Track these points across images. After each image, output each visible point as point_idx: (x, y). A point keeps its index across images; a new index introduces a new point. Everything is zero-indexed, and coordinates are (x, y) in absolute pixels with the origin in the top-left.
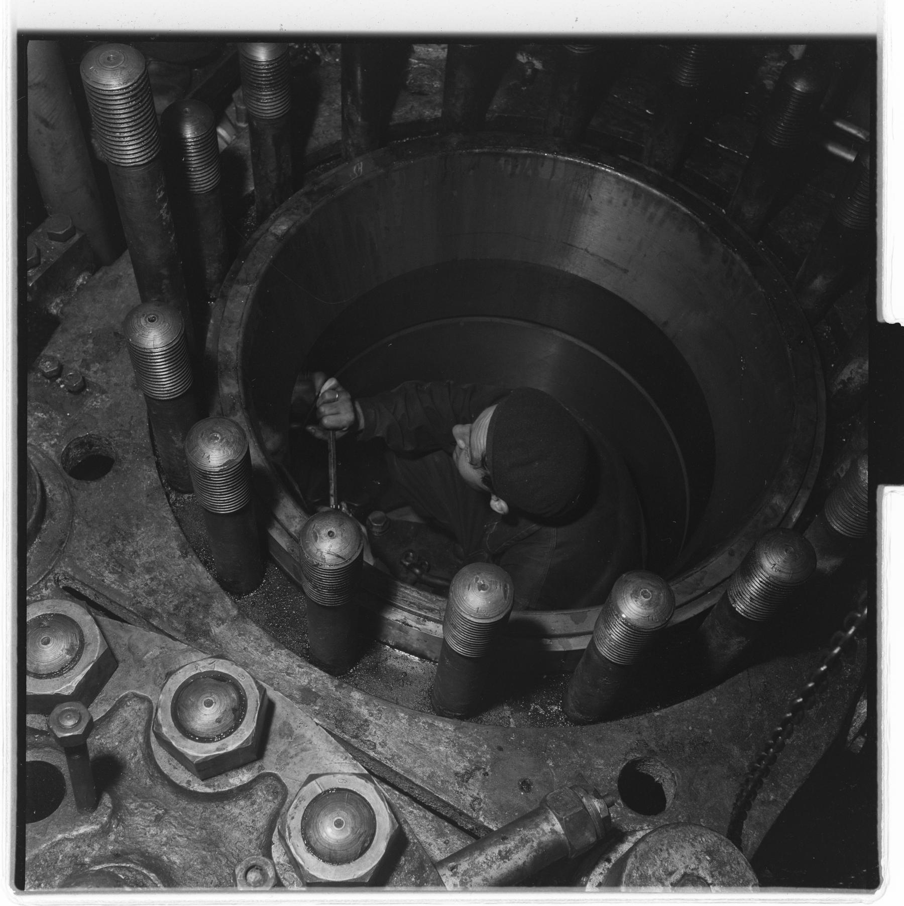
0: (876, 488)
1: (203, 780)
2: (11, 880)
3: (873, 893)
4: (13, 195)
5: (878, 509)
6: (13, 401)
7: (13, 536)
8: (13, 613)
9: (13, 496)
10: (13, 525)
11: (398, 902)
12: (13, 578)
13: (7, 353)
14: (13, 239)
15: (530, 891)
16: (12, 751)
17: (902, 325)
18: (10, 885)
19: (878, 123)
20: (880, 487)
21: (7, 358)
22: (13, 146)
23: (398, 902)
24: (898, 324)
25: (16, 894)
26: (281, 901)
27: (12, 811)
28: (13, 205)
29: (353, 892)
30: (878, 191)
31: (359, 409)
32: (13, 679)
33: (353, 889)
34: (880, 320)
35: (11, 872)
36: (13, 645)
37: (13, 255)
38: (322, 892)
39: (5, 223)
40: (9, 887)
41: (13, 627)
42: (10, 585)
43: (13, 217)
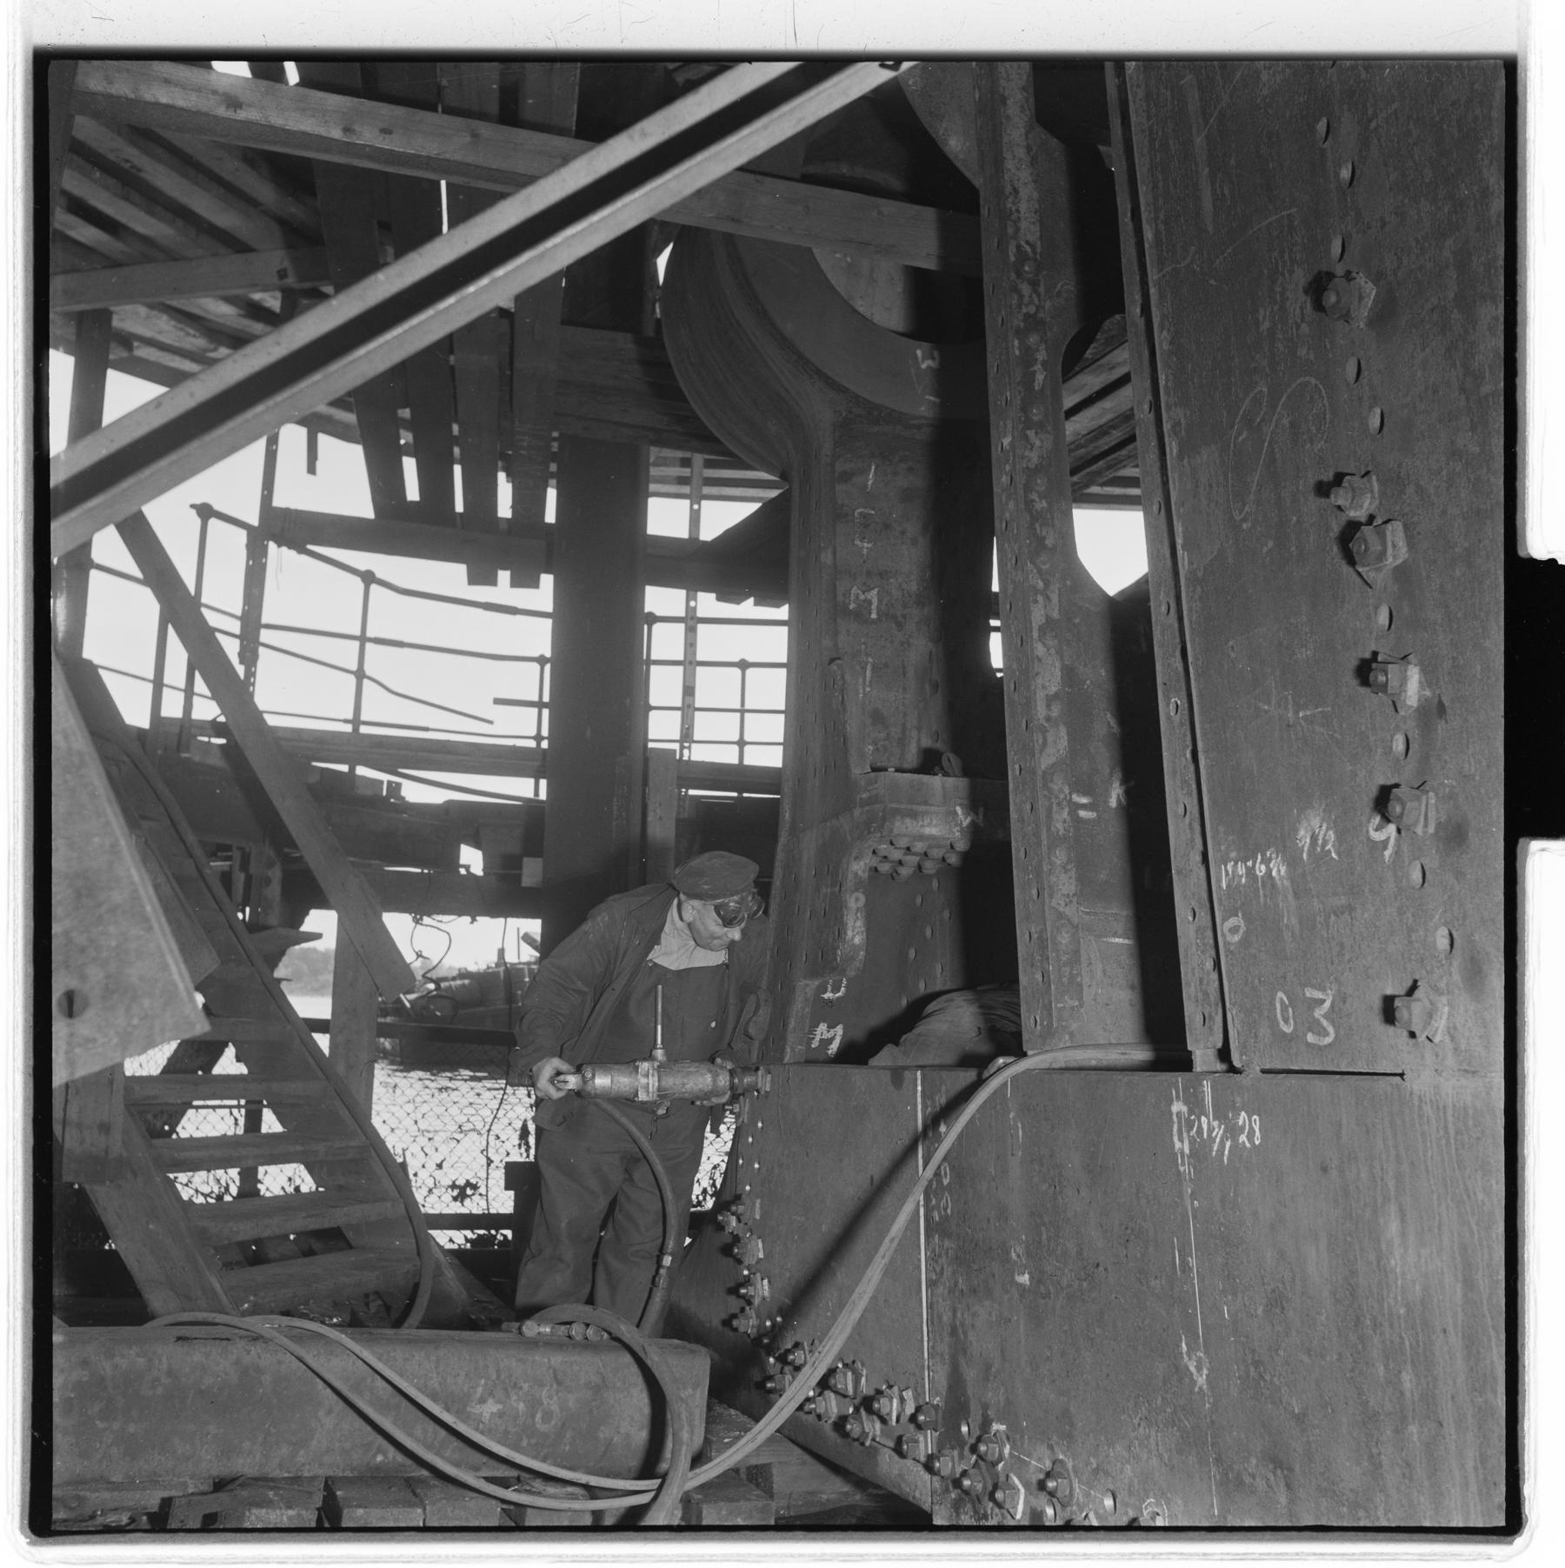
0: (1516, 843)
1: (398, 1324)
2: (22, 1519)
3: (1511, 1543)
4: (26, 338)
5: (1519, 880)
6: (26, 693)
7: (26, 926)
8: (26, 1059)
9: (25, 661)
10: (26, 906)
13: (15, 610)
14: (26, 413)
15: (919, 1539)
16: (25, 1297)
17: (1563, 561)
18: (22, 1528)
19: (1519, 214)
20: (1522, 841)
21: (16, 620)
22: (25, 950)
23: (212, 1561)
24: (1553, 561)
25: (31, 1543)
26: (488, 1557)
27: (24, 1399)
28: (26, 355)
29: (612, 1540)
30: (1519, 330)
31: (1095, 489)
33: (832, 1534)
34: (1521, 553)
36: (25, 1115)
37: (26, 442)
38: (843, 1540)
39: (11, 385)
40: (18, 1532)
41: (25, 1083)
42: (19, 1314)
43: (26, 376)
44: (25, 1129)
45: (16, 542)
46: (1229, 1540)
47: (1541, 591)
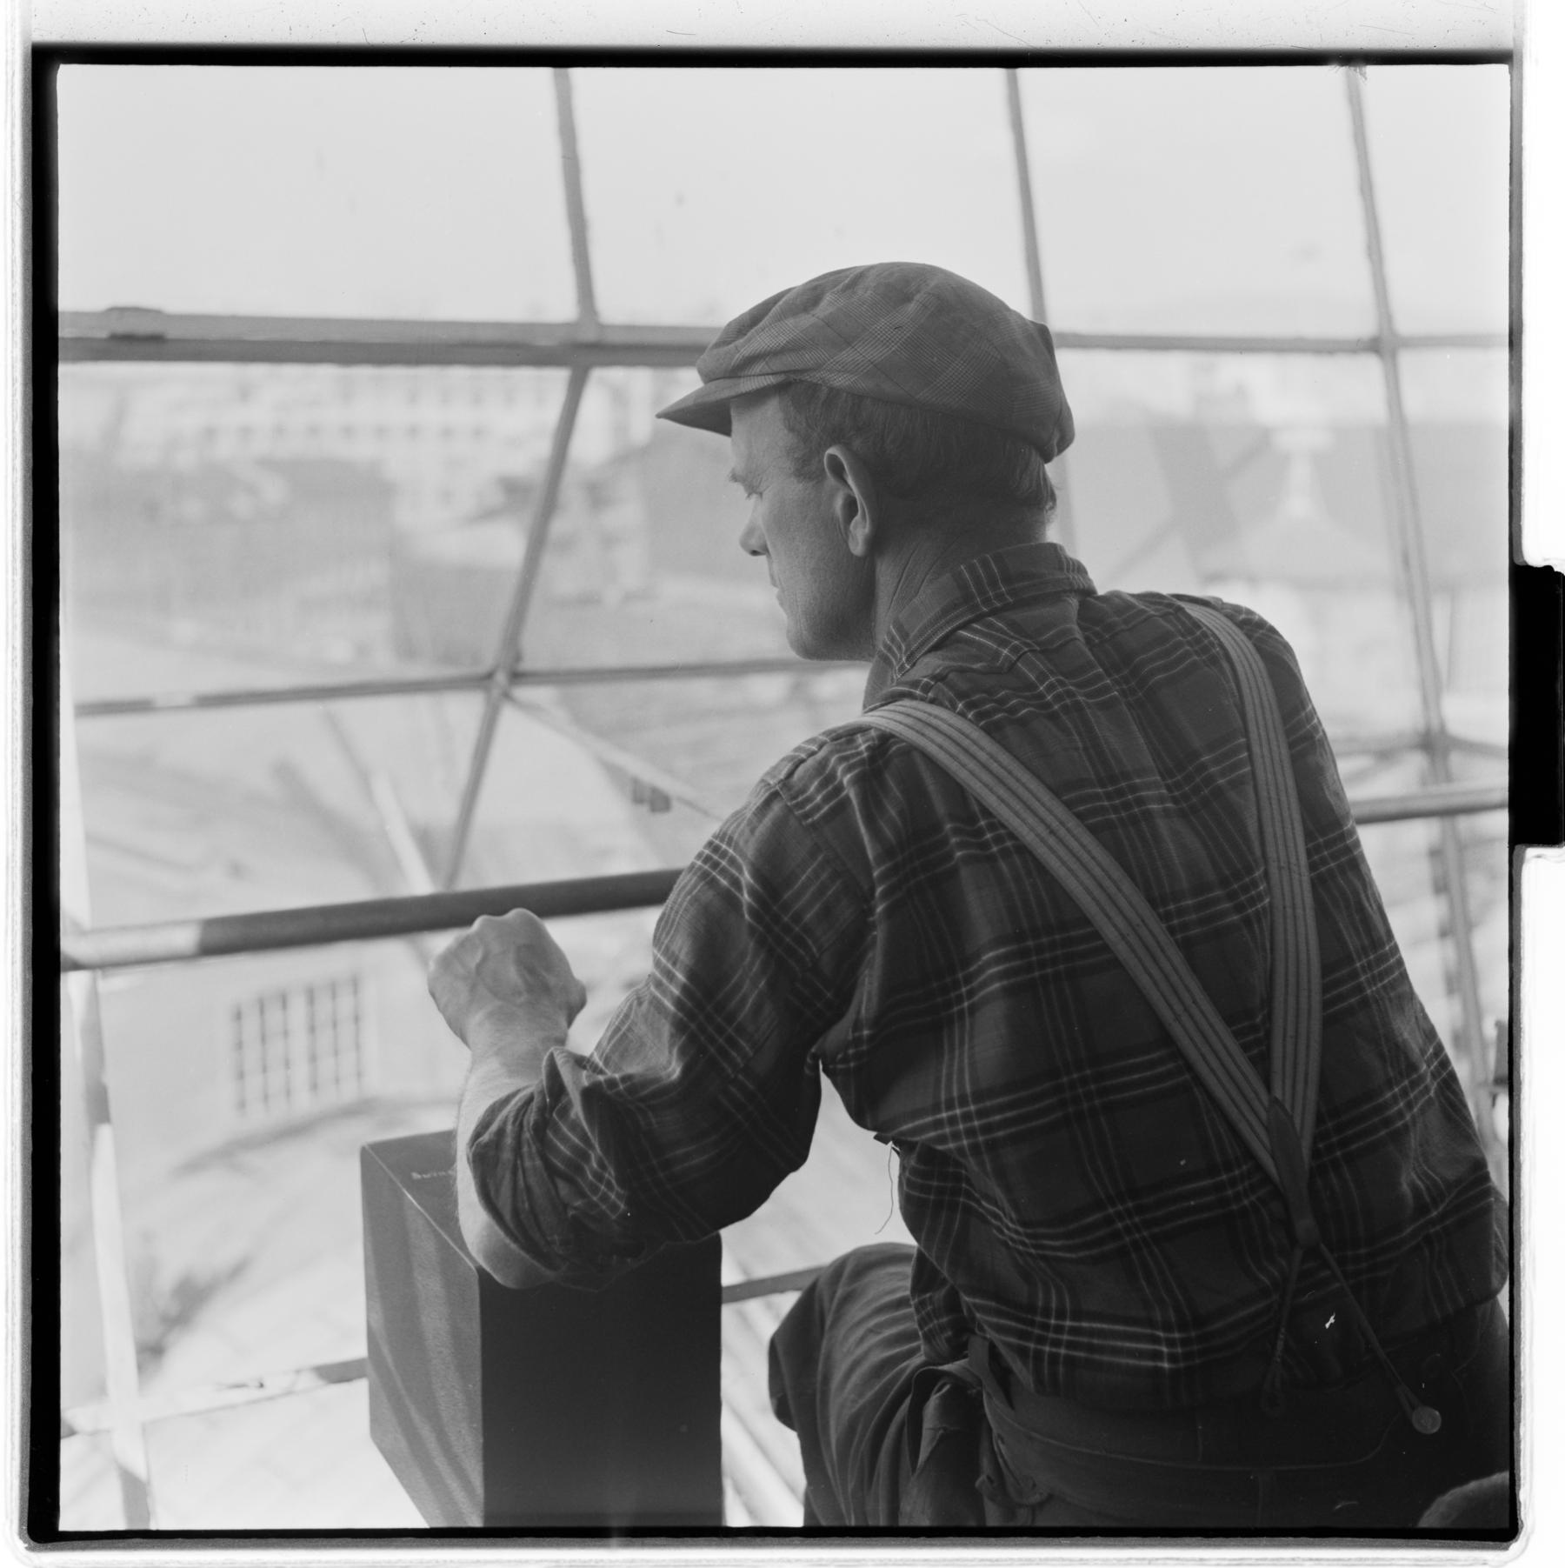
2: (21, 1524)
3: (1506, 1548)
11: (1030, 1561)
12: (25, 89)
13: (14, 616)
16: (24, 1303)
20: (1518, 847)
21: (14, 603)
23: (1030, 1561)
24: (1549, 569)
26: (527, 1562)
27: (23, 1405)
28: (25, 363)
32: (24, 1179)
35: (21, 1512)
36: (24, 1121)
38: (534, 1546)
40: (17, 1538)
44: (24, 1136)
45: (14, 548)
46: (325, 1547)
47: (1534, 589)
